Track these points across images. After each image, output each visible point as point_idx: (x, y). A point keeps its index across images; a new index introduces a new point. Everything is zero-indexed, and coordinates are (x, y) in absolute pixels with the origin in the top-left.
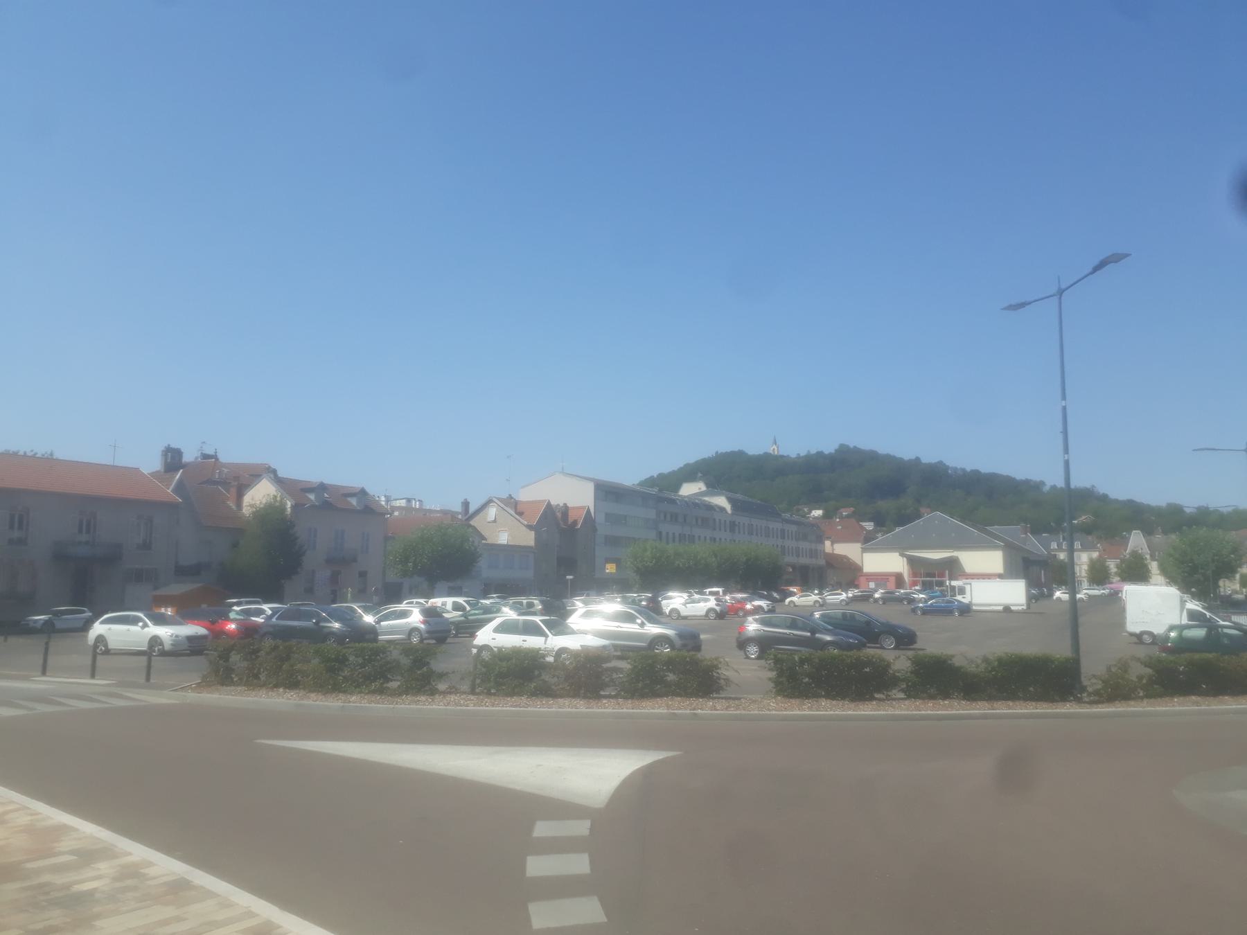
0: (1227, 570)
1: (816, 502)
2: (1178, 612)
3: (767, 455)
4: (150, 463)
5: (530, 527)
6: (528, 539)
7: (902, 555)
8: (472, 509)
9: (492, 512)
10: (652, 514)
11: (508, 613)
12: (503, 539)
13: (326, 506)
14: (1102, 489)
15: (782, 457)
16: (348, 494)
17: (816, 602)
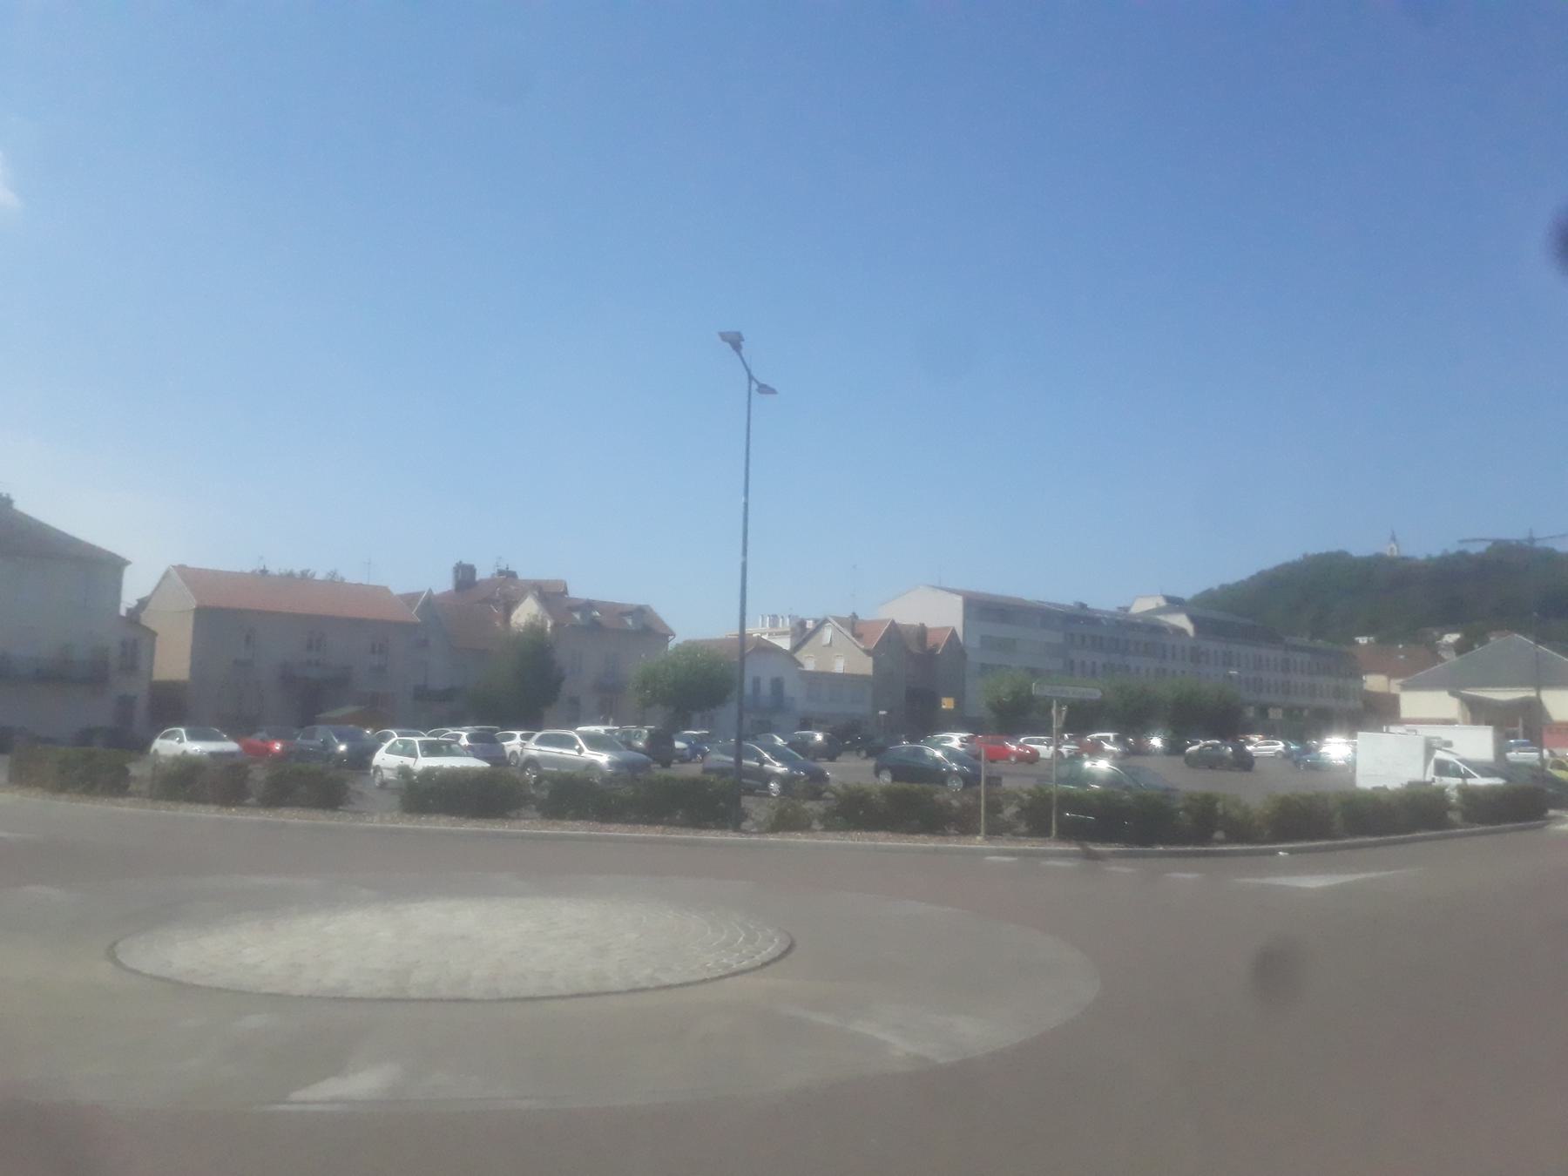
0: (802, 624)
1: (1450, 624)
5: (868, 652)
6: (866, 666)
7: (1452, 694)
8: (810, 625)
9: (827, 634)
11: (395, 737)
12: (839, 667)
13: (595, 627)
15: (1404, 558)
16: (621, 612)
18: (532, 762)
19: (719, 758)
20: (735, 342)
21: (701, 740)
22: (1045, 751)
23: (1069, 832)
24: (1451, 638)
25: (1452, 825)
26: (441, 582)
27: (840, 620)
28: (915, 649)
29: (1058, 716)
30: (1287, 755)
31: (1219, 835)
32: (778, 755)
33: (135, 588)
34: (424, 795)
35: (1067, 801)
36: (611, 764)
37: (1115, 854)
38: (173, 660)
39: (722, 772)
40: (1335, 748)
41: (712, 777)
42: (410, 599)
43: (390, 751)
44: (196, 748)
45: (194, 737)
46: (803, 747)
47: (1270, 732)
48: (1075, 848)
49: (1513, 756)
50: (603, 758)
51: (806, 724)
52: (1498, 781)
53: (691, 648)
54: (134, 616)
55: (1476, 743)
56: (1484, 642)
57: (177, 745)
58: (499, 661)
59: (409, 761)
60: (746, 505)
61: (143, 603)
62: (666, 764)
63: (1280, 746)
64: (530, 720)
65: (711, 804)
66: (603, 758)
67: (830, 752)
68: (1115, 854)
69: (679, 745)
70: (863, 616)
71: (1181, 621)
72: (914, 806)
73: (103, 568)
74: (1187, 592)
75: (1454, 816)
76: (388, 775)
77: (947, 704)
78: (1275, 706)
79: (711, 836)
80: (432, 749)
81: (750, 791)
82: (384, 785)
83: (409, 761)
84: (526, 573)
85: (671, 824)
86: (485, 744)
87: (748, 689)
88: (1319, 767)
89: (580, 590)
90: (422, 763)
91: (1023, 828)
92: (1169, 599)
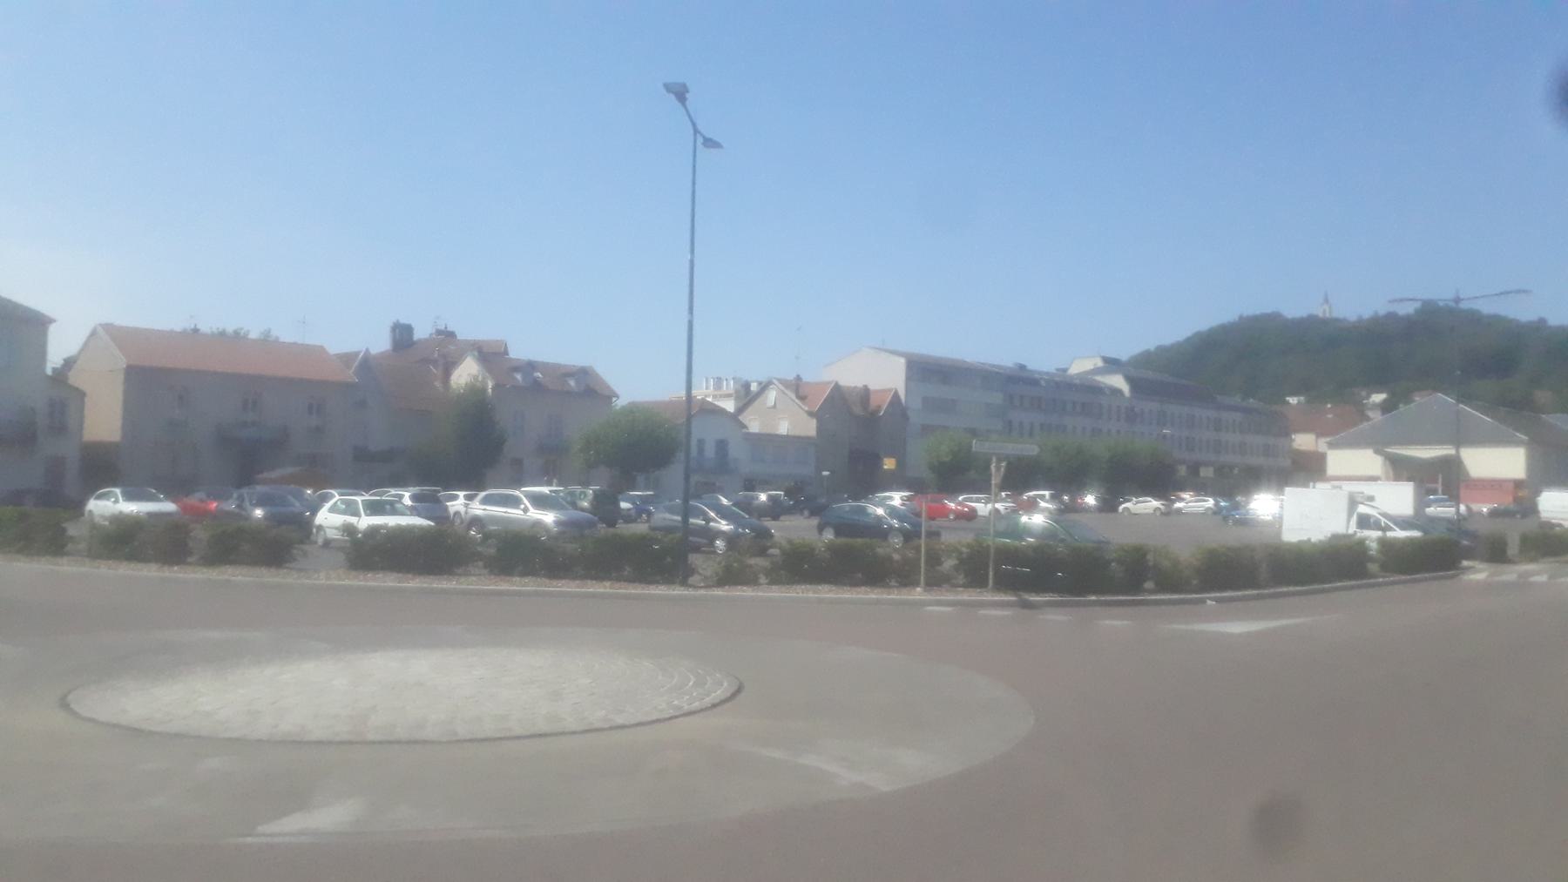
0: (747, 386)
2: (1344, 515)
4: (380, 343)
5: (811, 414)
6: (809, 428)
7: (1377, 452)
8: (754, 387)
9: (771, 396)
10: (997, 398)
11: (336, 497)
12: (783, 428)
13: (537, 387)
15: (1337, 320)
17: (1157, 509)
18: (476, 521)
19: (665, 516)
21: (646, 500)
22: (983, 508)
23: (1007, 583)
27: (785, 383)
28: (858, 410)
29: (996, 473)
30: (1217, 511)
31: (1149, 585)
32: (724, 513)
33: (60, 347)
34: (372, 553)
35: (1007, 555)
36: (558, 523)
38: (103, 420)
39: (669, 530)
40: (1263, 505)
41: (659, 535)
42: (347, 358)
43: (333, 510)
45: (130, 497)
46: (747, 506)
47: (1201, 489)
49: (1430, 510)
50: (549, 518)
51: (751, 485)
52: (1416, 534)
53: (632, 409)
54: (60, 377)
57: (111, 505)
58: (439, 425)
59: (353, 520)
61: (69, 363)
63: (1210, 502)
64: (472, 477)
66: (549, 518)
71: (1118, 382)
72: (857, 561)
75: (1373, 567)
76: (332, 534)
77: (889, 464)
78: (1206, 464)
80: (375, 508)
81: (697, 549)
82: (327, 543)
83: (353, 520)
84: (465, 333)
85: (618, 579)
86: (428, 504)
89: (520, 351)
90: (365, 522)
91: (961, 579)
92: (1106, 360)
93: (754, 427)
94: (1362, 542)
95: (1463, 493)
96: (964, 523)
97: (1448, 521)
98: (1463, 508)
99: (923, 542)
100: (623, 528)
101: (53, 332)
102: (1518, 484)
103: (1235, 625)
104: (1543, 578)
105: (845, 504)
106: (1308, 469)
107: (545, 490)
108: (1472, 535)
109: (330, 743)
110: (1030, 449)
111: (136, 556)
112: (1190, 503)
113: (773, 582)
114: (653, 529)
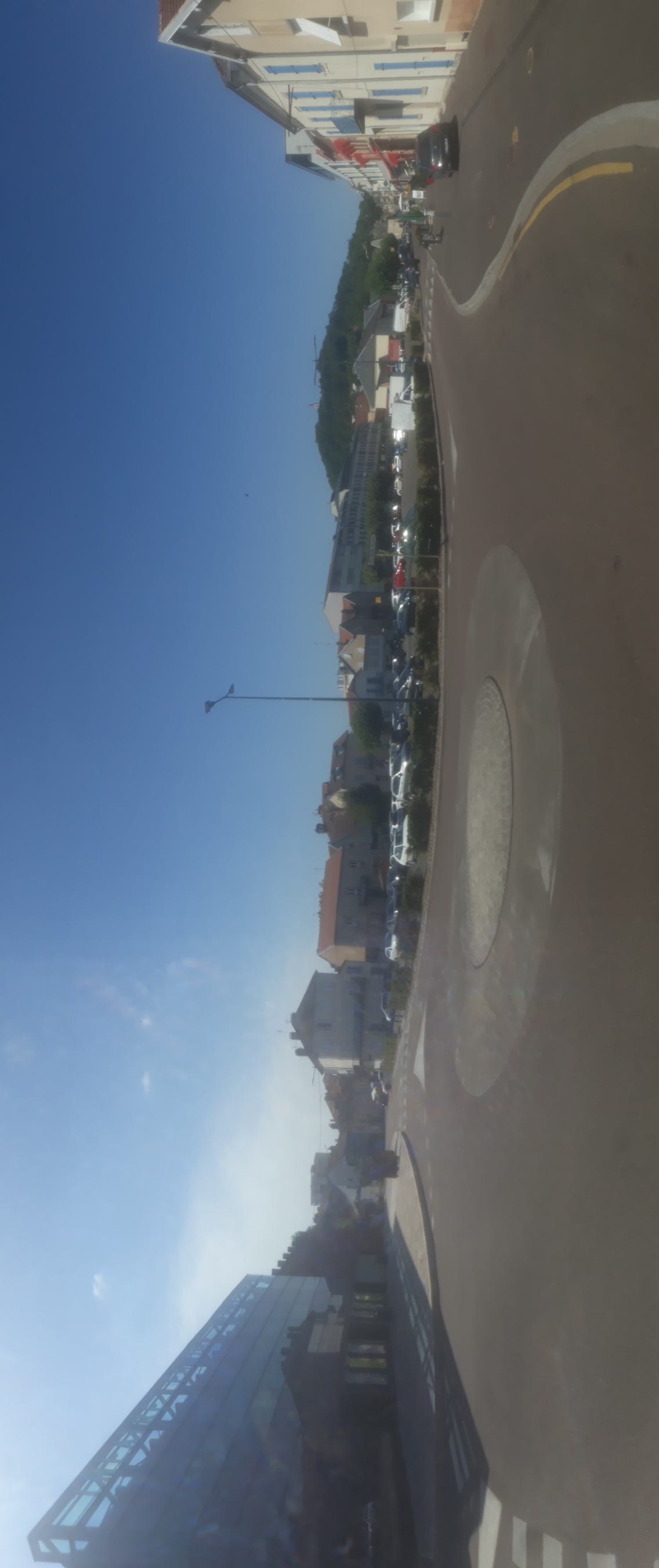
0: (342, 669)
3: (319, 411)
5: (355, 637)
6: (361, 638)
7: (377, 388)
8: (342, 665)
9: (346, 656)
12: (361, 650)
13: (343, 769)
14: (350, 236)
18: (406, 796)
19: (404, 710)
20: (209, 705)
21: (396, 718)
22: (399, 558)
23: (436, 549)
24: (354, 387)
25: (430, 397)
26: (325, 838)
27: (340, 649)
28: (353, 615)
29: (383, 554)
30: (401, 455)
31: (435, 487)
32: (403, 680)
33: (325, 968)
34: (420, 842)
35: (422, 550)
36: (407, 760)
37: (445, 531)
38: (355, 953)
39: (411, 708)
40: (398, 435)
41: (414, 712)
42: (332, 851)
43: (399, 858)
44: (394, 943)
45: (389, 944)
46: (400, 669)
47: (391, 460)
48: (443, 548)
49: (402, 370)
50: (405, 764)
51: (389, 666)
52: (412, 379)
53: (353, 723)
54: (338, 969)
55: (397, 384)
56: (356, 376)
57: (392, 950)
58: (359, 813)
59: (404, 850)
60: (286, 698)
61: (333, 966)
62: (408, 734)
63: (397, 457)
64: (388, 798)
65: (426, 714)
66: (405, 764)
67: (402, 656)
68: (445, 531)
69: (399, 728)
70: (337, 639)
71: (342, 495)
72: (425, 618)
73: (318, 982)
74: (330, 492)
75: (426, 396)
76: (411, 858)
77: (378, 600)
78: (380, 458)
79: (441, 715)
80: (399, 840)
81: (420, 694)
82: (415, 860)
83: (404, 850)
84: (319, 802)
85: (435, 731)
86: (398, 818)
87: (373, 696)
88: (405, 442)
89: (327, 777)
90: (405, 844)
91: (434, 570)
92: (332, 500)
93: (360, 665)
94: (416, 400)
95: (392, 359)
96: (407, 567)
97: (406, 367)
98: (401, 359)
99: (416, 588)
100: (411, 727)
101: (320, 971)
102: (391, 338)
103: (453, 455)
104: (430, 334)
105: (400, 628)
106: (384, 418)
107: (391, 765)
108: (412, 358)
109: (509, 860)
110: (373, 539)
111: (415, 942)
112: (397, 465)
113: (437, 658)
114: (411, 713)
